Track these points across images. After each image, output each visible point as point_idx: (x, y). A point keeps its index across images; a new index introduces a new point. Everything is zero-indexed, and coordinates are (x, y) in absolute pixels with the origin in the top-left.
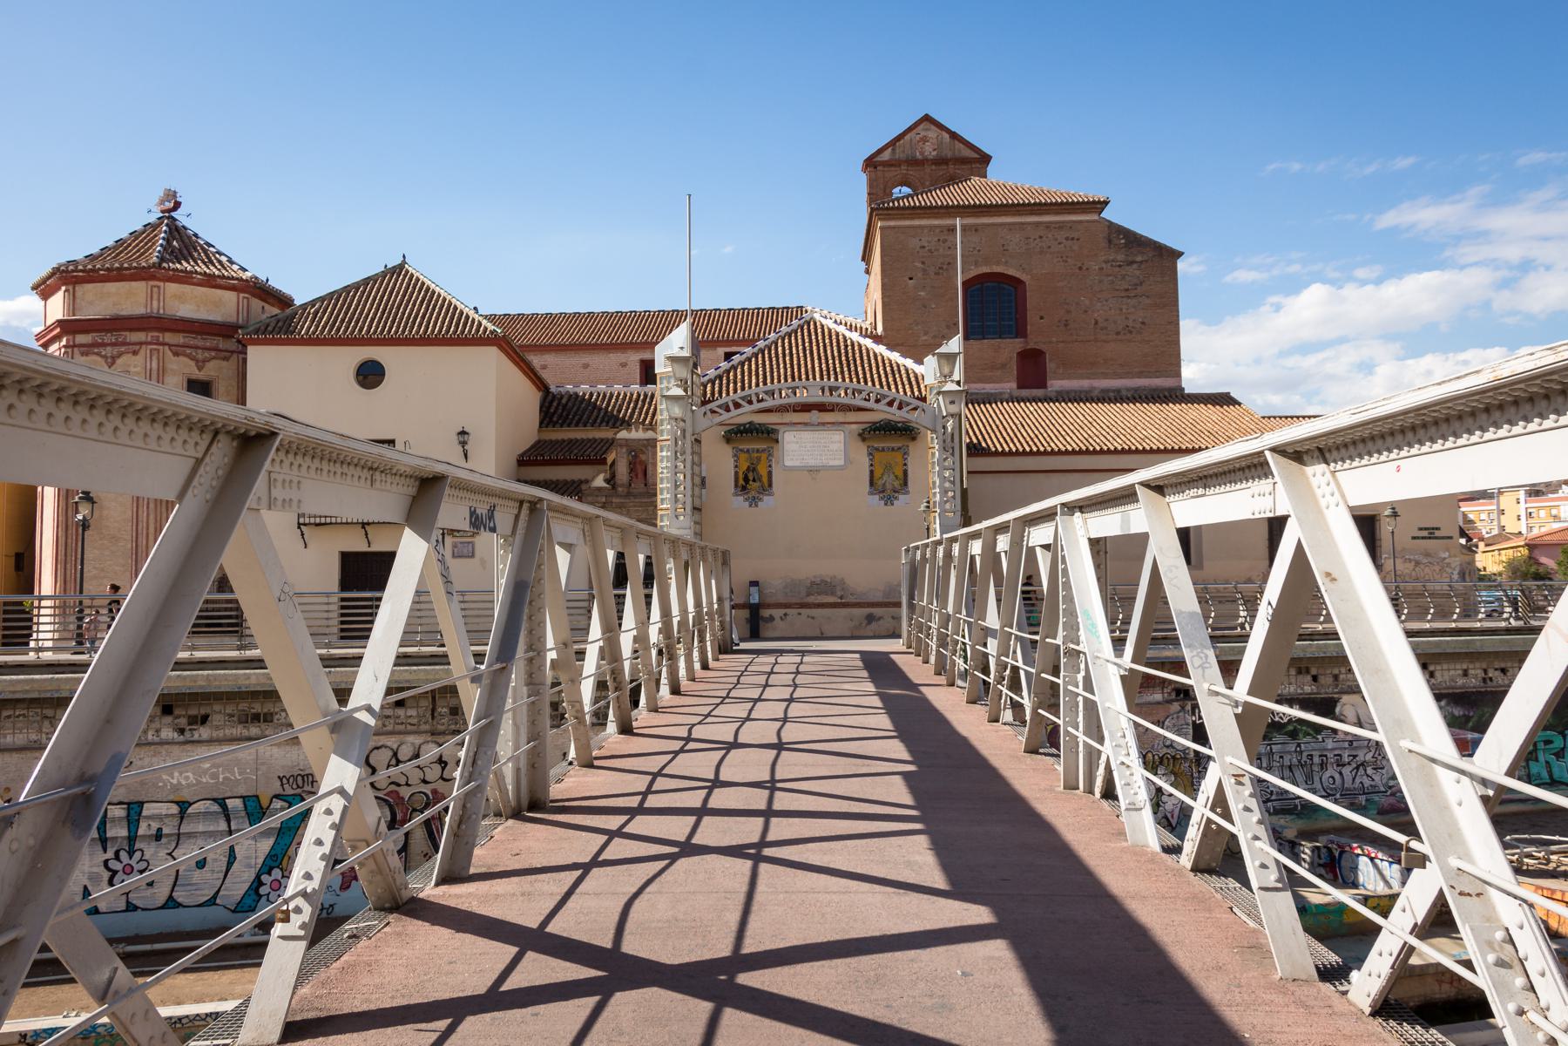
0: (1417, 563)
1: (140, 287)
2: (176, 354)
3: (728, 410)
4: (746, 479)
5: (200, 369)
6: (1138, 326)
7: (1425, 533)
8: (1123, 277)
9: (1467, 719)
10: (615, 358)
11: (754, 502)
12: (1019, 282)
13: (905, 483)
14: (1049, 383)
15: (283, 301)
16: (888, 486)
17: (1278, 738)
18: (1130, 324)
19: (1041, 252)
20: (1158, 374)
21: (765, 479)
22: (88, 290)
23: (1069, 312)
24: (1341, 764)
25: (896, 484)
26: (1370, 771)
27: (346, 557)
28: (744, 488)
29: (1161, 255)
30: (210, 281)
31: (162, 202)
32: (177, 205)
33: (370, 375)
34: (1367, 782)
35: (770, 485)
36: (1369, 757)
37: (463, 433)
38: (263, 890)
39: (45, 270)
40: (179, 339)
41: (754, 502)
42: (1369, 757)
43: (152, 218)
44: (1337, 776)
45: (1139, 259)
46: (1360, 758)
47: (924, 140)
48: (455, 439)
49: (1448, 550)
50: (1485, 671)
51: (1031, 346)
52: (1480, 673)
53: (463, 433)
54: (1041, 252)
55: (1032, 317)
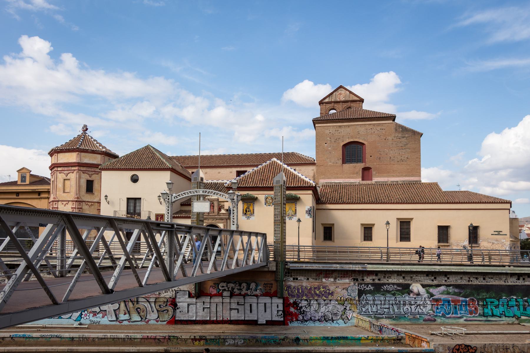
0: (493, 243)
1: (61, 161)
2: (83, 173)
4: (246, 211)
5: (90, 177)
6: (405, 159)
7: (496, 233)
8: (401, 142)
9: (460, 293)
10: (228, 170)
11: (248, 218)
13: (296, 213)
14: (373, 178)
15: (115, 157)
16: (290, 214)
17: (388, 295)
18: (403, 158)
19: (371, 134)
20: (413, 176)
22: (61, 155)
23: (380, 154)
24: (411, 305)
25: (293, 213)
26: (422, 307)
27: (371, 240)
28: (245, 214)
30: (93, 152)
31: (83, 128)
32: (87, 129)
33: (135, 179)
34: (420, 311)
36: (421, 303)
37: (106, 196)
38: (83, 316)
39: (50, 150)
40: (85, 169)
41: (248, 218)
42: (421, 303)
43: (80, 134)
44: (409, 308)
45: (407, 136)
46: (418, 303)
47: (340, 94)
48: (157, 198)
49: (505, 239)
50: (469, 278)
51: (367, 166)
53: (106, 196)
54: (371, 134)
55: (367, 156)
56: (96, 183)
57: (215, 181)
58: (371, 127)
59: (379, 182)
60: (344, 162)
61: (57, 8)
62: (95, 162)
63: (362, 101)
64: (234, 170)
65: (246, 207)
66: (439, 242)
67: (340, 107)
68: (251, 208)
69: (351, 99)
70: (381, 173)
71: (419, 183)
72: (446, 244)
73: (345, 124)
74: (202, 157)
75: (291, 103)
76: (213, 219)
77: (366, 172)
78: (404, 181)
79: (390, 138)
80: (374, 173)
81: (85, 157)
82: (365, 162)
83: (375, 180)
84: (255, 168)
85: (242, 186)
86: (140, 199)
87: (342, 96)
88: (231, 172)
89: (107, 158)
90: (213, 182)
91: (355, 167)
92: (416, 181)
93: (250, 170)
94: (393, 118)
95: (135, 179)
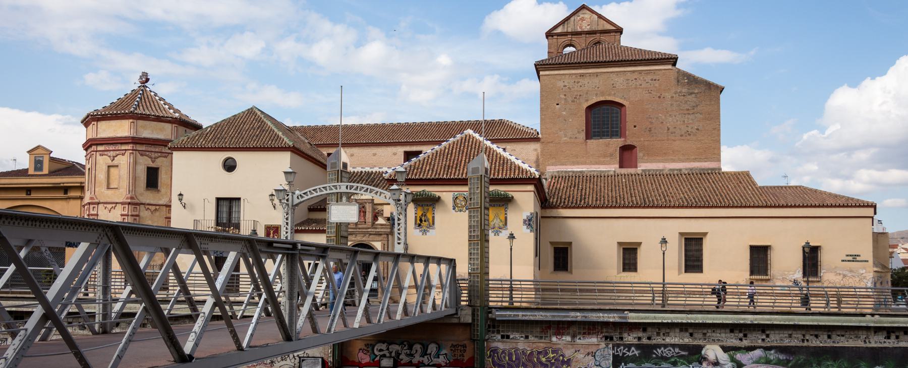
0: (845, 276)
2: (142, 155)
3: (302, 197)
4: (421, 220)
5: (153, 162)
7: (850, 258)
10: (390, 150)
11: (425, 232)
12: (621, 105)
13: (506, 224)
14: (639, 165)
15: (196, 127)
19: (636, 88)
20: (706, 159)
21: (431, 221)
22: (103, 125)
23: (651, 123)
25: (501, 225)
28: (420, 225)
29: (710, 88)
30: (158, 119)
31: (141, 78)
32: (147, 80)
33: (229, 166)
35: (433, 224)
37: (180, 195)
39: (84, 115)
40: (143, 148)
41: (425, 232)
43: (136, 87)
45: (696, 91)
47: (583, 19)
48: (268, 198)
49: (864, 268)
50: (804, 336)
51: (629, 143)
52: (801, 337)
53: (180, 195)
54: (636, 88)
55: (629, 125)
57: (368, 169)
58: (636, 75)
59: (649, 170)
63: (620, 31)
64: (401, 150)
65: (420, 213)
66: (752, 273)
67: (582, 42)
68: (429, 216)
69: (600, 28)
70: (652, 154)
71: (717, 171)
72: (765, 277)
74: (346, 127)
76: (365, 234)
77: (627, 154)
79: (668, 95)
80: (640, 155)
81: (144, 127)
82: (625, 137)
83: (642, 166)
84: (437, 147)
85: (413, 177)
86: (239, 199)
87: (585, 23)
88: (395, 154)
89: (182, 129)
90: (363, 170)
91: (607, 145)
93: (427, 150)
95: (229, 166)
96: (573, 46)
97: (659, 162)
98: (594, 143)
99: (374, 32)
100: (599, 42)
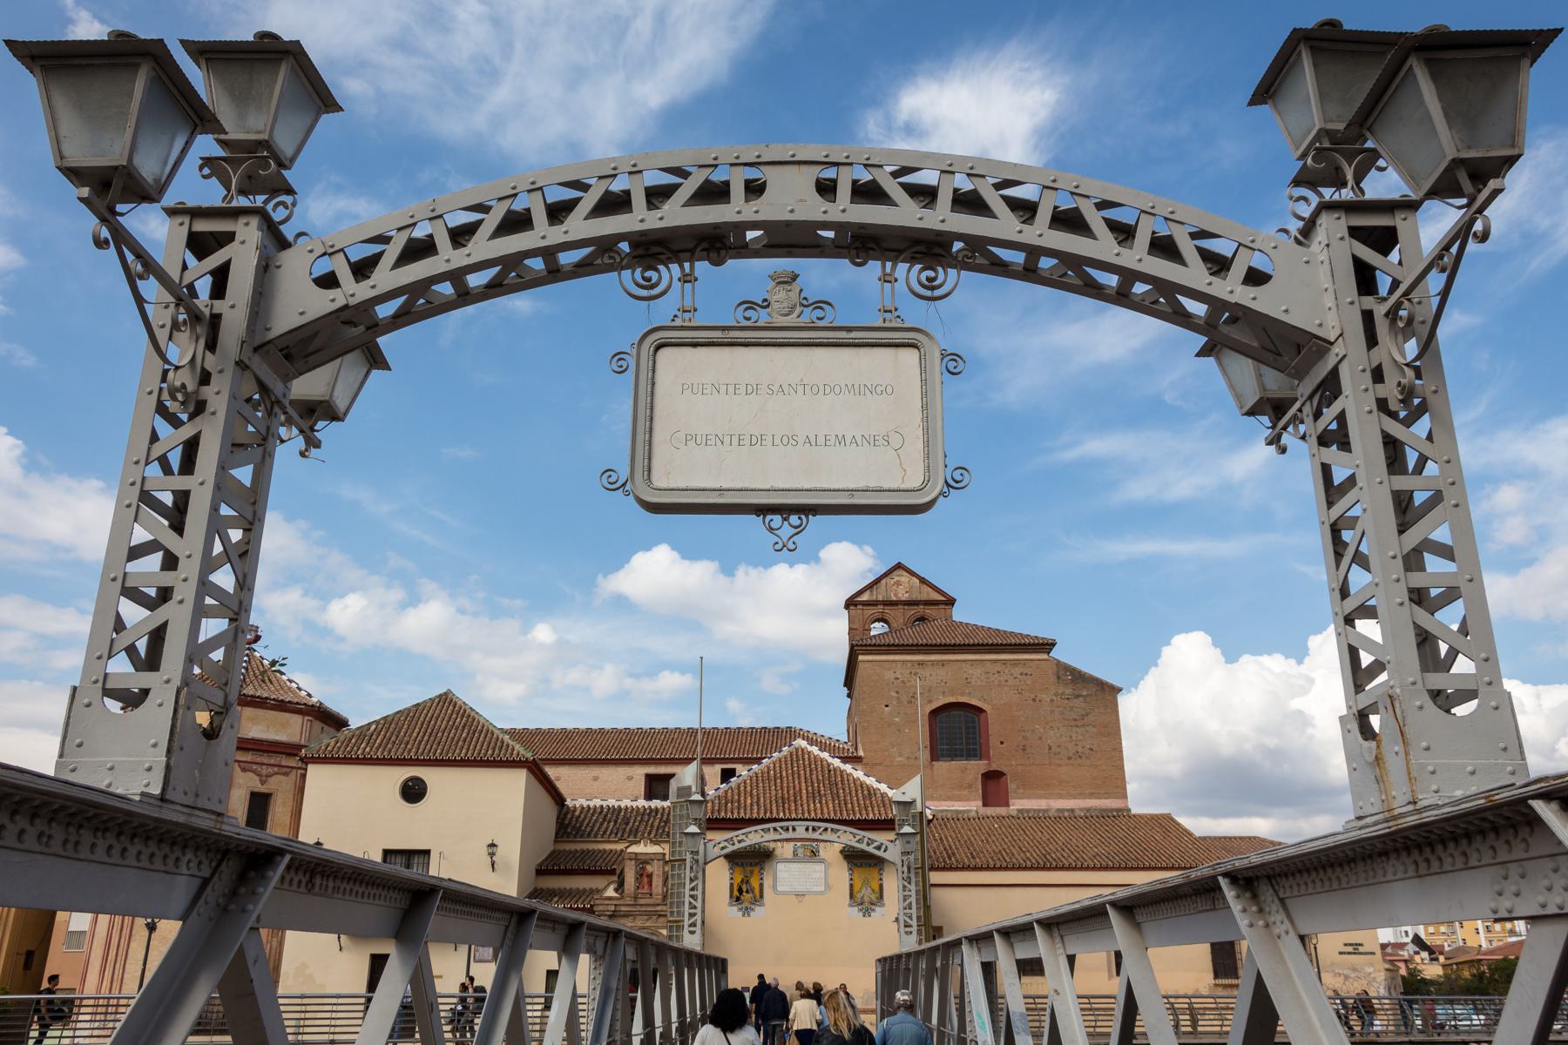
0: (1347, 977)
2: (244, 770)
4: (740, 891)
5: (263, 783)
7: (1350, 949)
10: (622, 772)
11: (747, 912)
12: (980, 710)
13: (881, 896)
15: (338, 723)
20: (1107, 796)
21: (757, 891)
23: (1025, 738)
25: (873, 897)
28: (738, 899)
30: (282, 706)
33: (413, 792)
35: (761, 896)
37: (493, 845)
41: (747, 912)
47: (898, 583)
48: (485, 851)
49: (1372, 965)
51: (994, 767)
53: (493, 845)
55: (994, 741)
56: (279, 801)
57: (612, 802)
58: (999, 667)
59: (1028, 811)
60: (935, 756)
61: (1088, 269)
62: (282, 737)
63: (951, 602)
64: (640, 772)
65: (738, 879)
66: (1216, 976)
67: (899, 616)
68: (755, 883)
69: (924, 597)
70: (1033, 786)
71: (1124, 813)
72: (1234, 982)
73: (891, 657)
74: (707, 733)
75: (621, 604)
76: (649, 915)
78: (1088, 810)
79: (1046, 697)
80: (1012, 786)
81: (254, 720)
82: (988, 758)
83: (1017, 805)
84: (755, 767)
85: (729, 815)
86: (428, 852)
87: (902, 588)
88: (630, 778)
89: (318, 725)
90: (605, 804)
91: (964, 771)
92: (1118, 810)
93: (742, 770)
94: (1047, 646)
95: (413, 792)
96: (885, 621)
97: (1040, 797)
98: (942, 766)
99: (428, 586)
100: (922, 619)
